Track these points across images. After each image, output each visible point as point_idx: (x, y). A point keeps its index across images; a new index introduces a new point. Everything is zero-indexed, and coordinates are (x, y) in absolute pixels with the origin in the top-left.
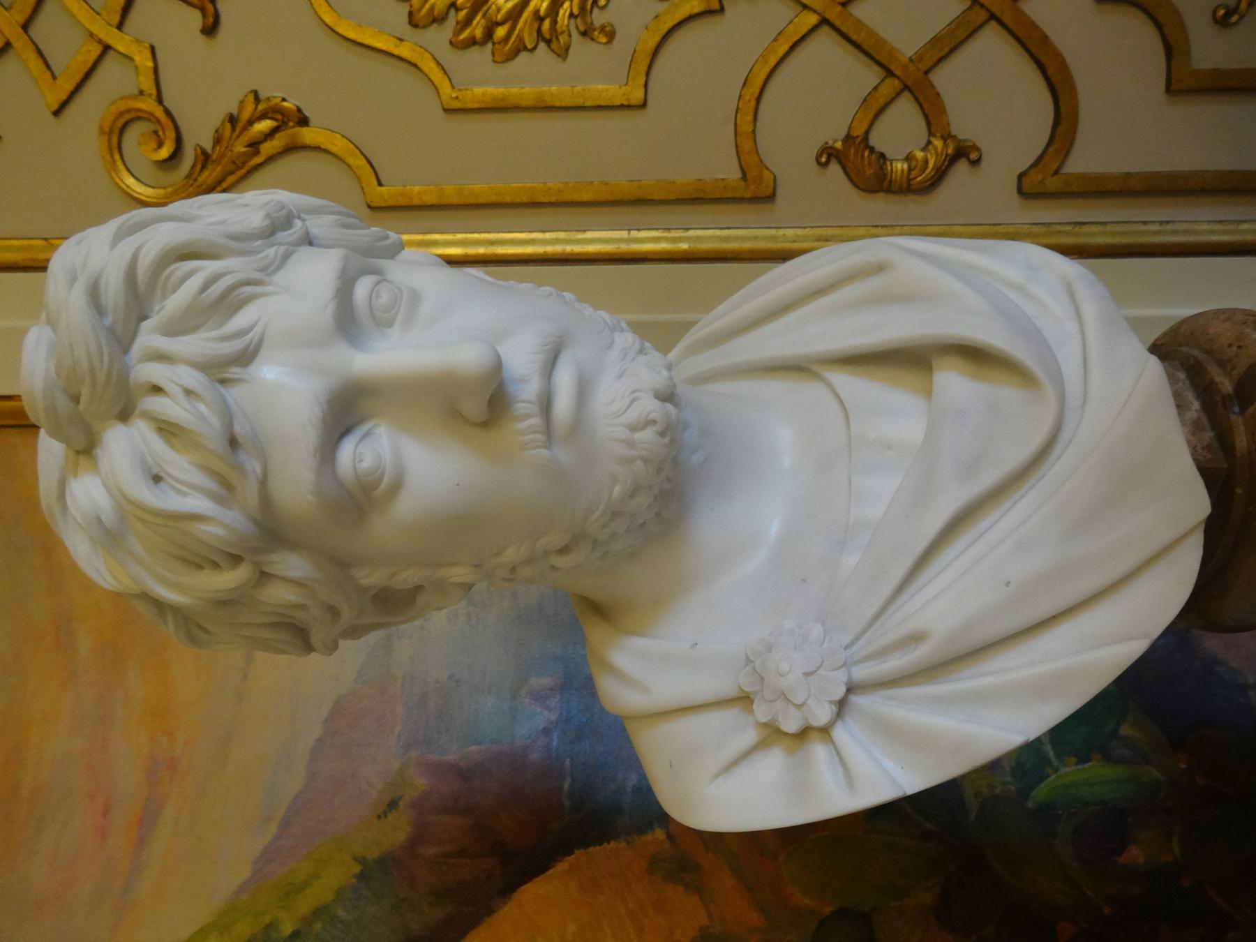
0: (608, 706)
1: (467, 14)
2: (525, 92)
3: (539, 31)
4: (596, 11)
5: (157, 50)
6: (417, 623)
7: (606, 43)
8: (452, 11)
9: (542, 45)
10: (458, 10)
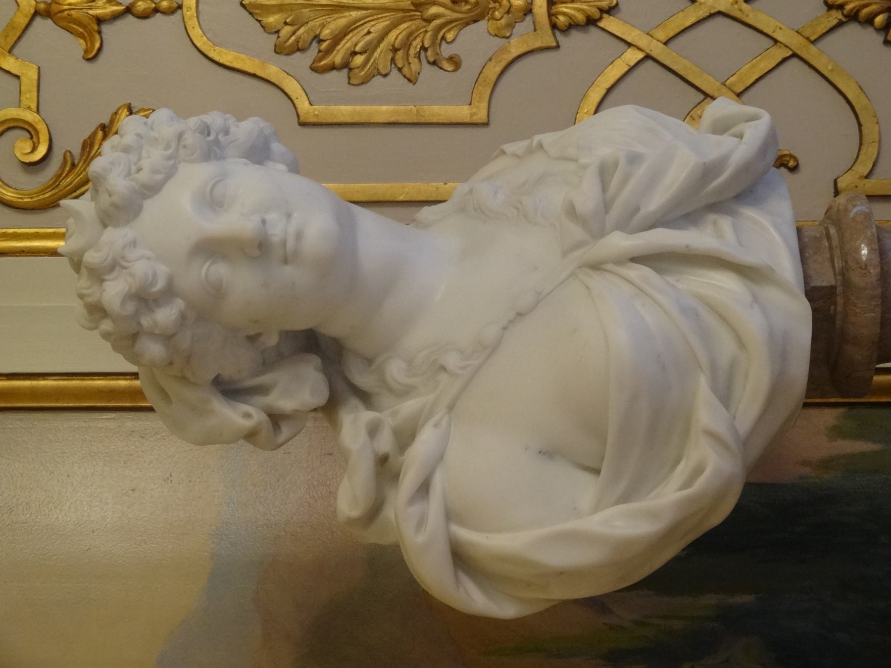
0: (324, 404)
1: (432, 35)
2: (383, 111)
3: (393, 60)
4: (444, 45)
5: (41, 68)
6: (227, 51)
7: (454, 71)
8: (314, 44)
9: (395, 72)
10: (321, 41)
